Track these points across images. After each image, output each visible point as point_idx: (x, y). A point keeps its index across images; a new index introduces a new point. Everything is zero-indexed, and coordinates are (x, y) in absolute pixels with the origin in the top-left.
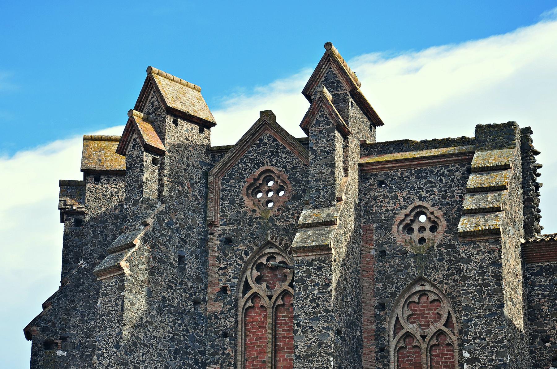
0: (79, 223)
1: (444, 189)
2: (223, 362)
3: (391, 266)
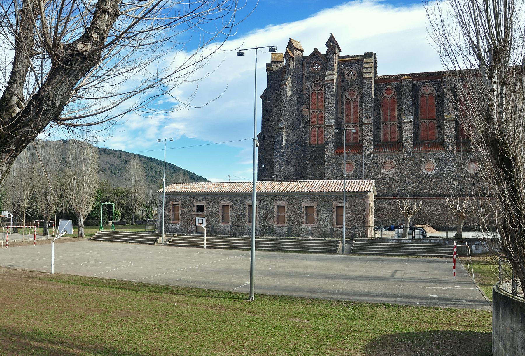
0: (271, 73)
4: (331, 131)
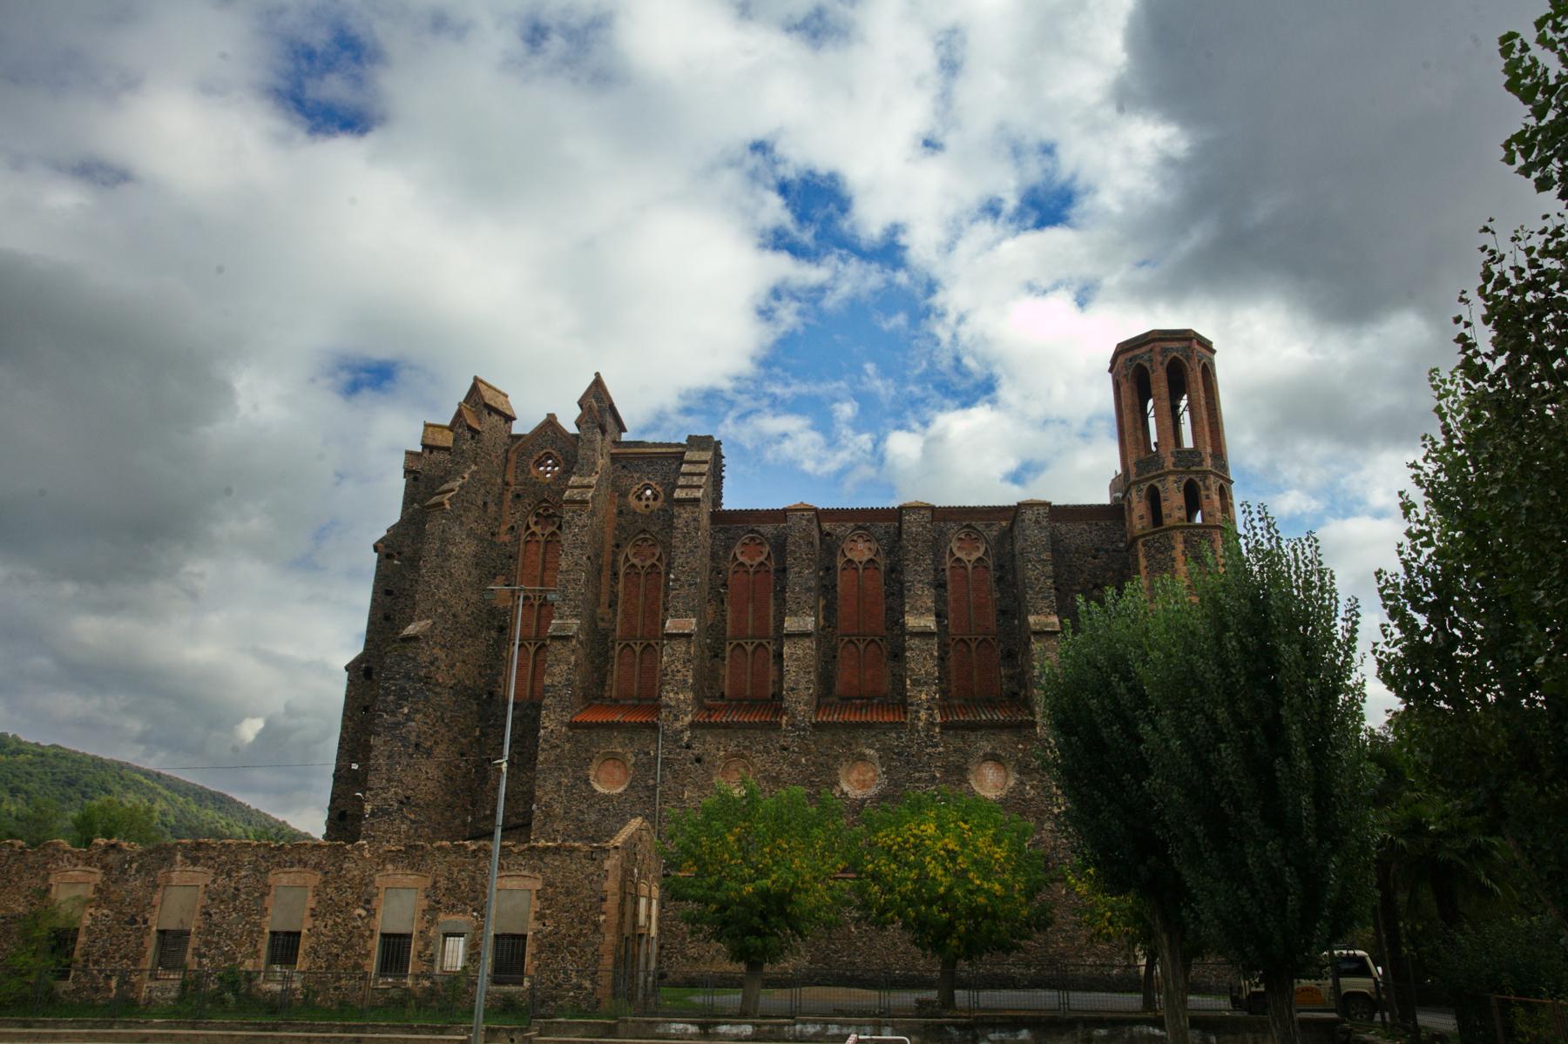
4: (566, 652)
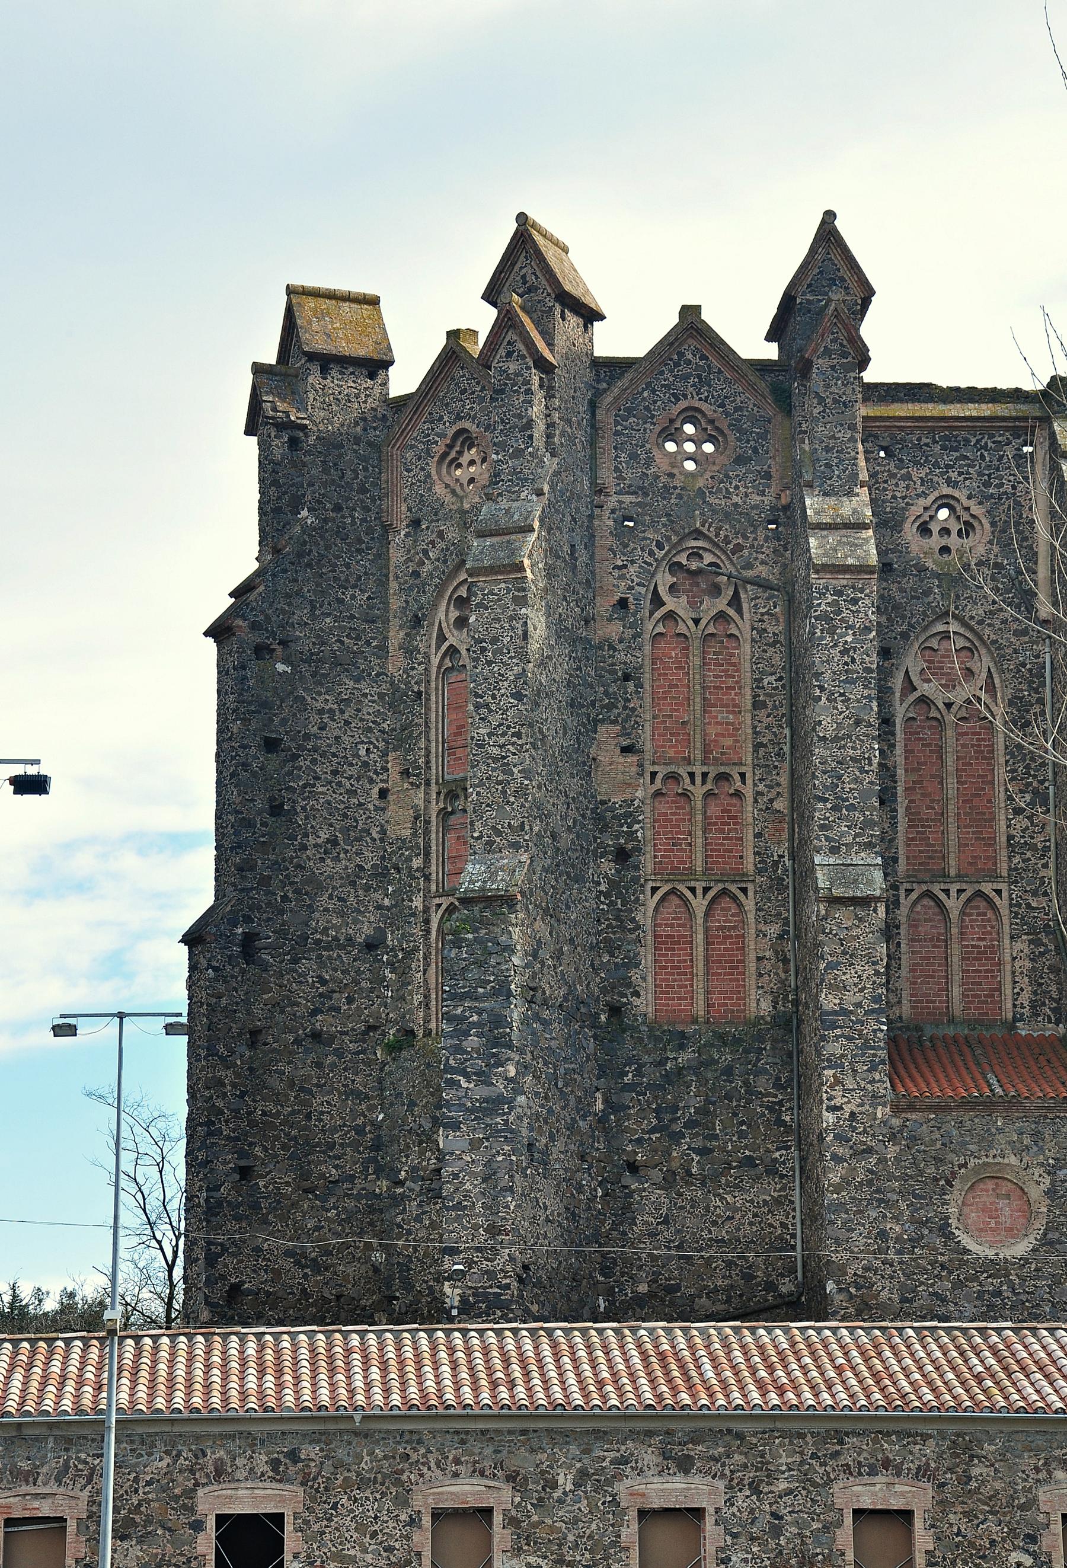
1: (987, 472)
2: (625, 720)
3: (902, 590)
